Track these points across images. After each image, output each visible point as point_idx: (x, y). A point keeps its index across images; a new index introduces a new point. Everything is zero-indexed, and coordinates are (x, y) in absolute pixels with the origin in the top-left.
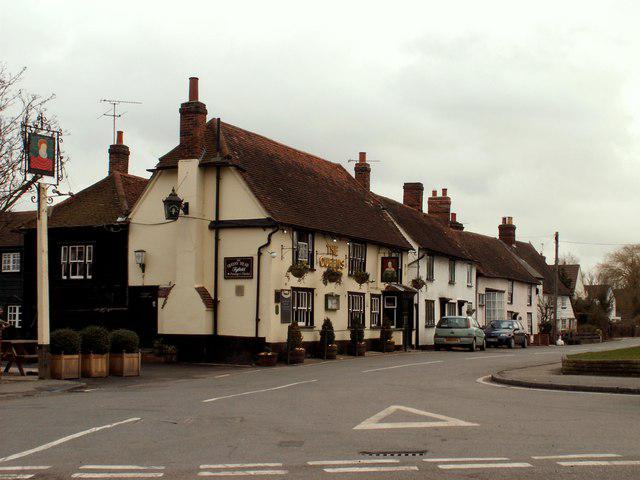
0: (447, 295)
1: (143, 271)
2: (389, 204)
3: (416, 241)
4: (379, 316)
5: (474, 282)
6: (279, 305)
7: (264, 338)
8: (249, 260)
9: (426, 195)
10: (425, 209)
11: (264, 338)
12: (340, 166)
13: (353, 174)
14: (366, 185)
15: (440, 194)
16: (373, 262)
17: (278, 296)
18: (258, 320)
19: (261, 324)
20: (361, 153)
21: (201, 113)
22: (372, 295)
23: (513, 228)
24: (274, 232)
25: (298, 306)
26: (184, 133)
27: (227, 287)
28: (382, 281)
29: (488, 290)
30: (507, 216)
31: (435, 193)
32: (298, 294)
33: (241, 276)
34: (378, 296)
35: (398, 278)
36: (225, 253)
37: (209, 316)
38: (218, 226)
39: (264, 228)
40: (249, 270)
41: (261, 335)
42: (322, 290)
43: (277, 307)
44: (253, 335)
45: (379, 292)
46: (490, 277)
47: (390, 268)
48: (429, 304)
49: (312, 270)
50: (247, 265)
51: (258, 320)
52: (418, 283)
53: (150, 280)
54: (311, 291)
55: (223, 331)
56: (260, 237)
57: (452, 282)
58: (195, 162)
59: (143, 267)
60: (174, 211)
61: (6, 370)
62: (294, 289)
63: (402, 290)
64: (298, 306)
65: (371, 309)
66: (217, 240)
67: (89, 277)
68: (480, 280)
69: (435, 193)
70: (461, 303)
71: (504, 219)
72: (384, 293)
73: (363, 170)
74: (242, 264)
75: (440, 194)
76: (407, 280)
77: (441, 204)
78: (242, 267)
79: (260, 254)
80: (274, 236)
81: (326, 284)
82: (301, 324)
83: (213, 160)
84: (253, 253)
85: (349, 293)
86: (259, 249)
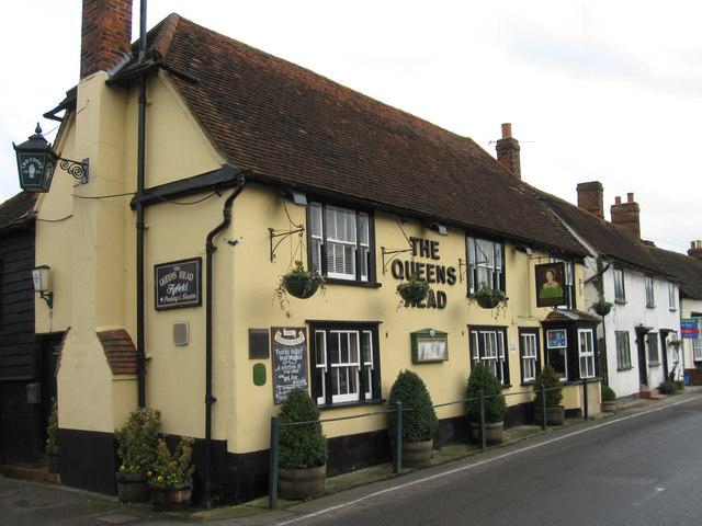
0: (647, 325)
1: (51, 307)
4: (538, 363)
6: (268, 363)
8: (191, 264)
9: (608, 202)
10: (608, 217)
13: (494, 154)
15: (624, 200)
16: (520, 271)
17: (260, 343)
18: (210, 401)
19: (218, 410)
20: (503, 125)
22: (522, 330)
27: (161, 326)
28: (539, 306)
30: (695, 240)
31: (618, 199)
32: (481, 336)
33: (182, 306)
34: (534, 330)
35: (567, 296)
36: (160, 253)
37: (129, 387)
38: (147, 200)
40: (194, 287)
41: (218, 435)
42: (400, 322)
44: (203, 436)
45: (537, 325)
47: (551, 284)
48: (622, 338)
50: (190, 277)
51: (210, 401)
52: (603, 309)
56: (209, 212)
57: (650, 306)
61: (329, 400)
64: (332, 358)
65: (522, 353)
66: (142, 229)
68: (685, 302)
69: (618, 199)
70: (664, 333)
71: (693, 243)
72: (546, 325)
73: (508, 147)
74: (183, 275)
76: (584, 301)
77: (628, 212)
79: (211, 249)
80: (236, 202)
81: (380, 285)
84: (199, 250)
85: (471, 327)
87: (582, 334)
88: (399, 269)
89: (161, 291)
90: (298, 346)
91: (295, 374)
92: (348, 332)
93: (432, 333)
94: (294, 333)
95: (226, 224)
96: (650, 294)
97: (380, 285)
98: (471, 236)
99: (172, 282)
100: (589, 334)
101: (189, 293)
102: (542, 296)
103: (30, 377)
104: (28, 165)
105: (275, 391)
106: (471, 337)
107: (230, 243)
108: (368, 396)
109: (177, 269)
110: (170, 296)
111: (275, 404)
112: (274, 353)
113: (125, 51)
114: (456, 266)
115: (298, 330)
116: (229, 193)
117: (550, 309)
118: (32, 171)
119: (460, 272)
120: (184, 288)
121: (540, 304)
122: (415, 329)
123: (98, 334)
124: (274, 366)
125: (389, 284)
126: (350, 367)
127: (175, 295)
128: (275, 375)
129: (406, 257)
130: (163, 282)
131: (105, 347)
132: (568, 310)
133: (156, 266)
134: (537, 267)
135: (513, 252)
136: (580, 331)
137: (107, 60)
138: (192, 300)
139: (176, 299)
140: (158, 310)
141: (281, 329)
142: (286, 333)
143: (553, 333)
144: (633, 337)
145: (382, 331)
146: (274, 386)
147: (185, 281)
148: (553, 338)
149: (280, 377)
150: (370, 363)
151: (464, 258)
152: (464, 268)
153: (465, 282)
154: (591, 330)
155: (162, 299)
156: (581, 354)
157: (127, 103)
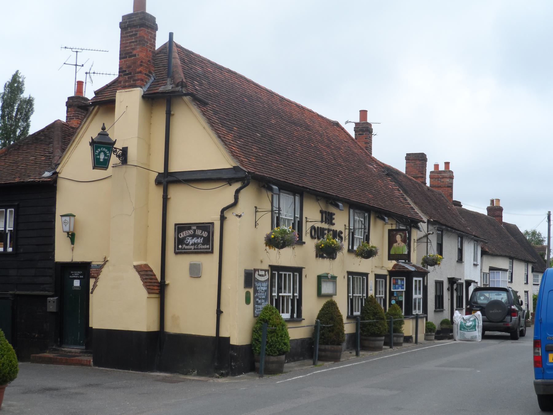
1: (73, 242)
2: (390, 172)
3: (425, 212)
5: (479, 262)
6: (251, 291)
7: (228, 339)
8: (207, 227)
9: (430, 168)
11: (228, 339)
12: (337, 124)
13: (353, 134)
14: (368, 147)
18: (219, 312)
19: (224, 319)
21: (147, 27)
22: (377, 276)
23: (501, 209)
24: (241, 188)
25: (279, 290)
26: (124, 54)
29: (491, 269)
31: (437, 166)
32: (280, 276)
34: (383, 277)
37: (155, 304)
39: (230, 181)
40: (208, 240)
41: (224, 334)
43: (248, 294)
44: (214, 334)
45: (385, 272)
46: (494, 255)
48: (439, 284)
49: (301, 242)
50: (205, 234)
51: (219, 312)
53: (79, 257)
54: (299, 270)
55: (170, 328)
58: (137, 93)
59: (72, 236)
60: (102, 157)
62: (273, 268)
63: (413, 269)
66: (165, 199)
67: (10, 250)
68: (485, 258)
69: (437, 166)
70: (469, 283)
71: (492, 201)
72: (392, 273)
74: (199, 232)
75: (442, 168)
76: (416, 259)
78: (198, 237)
79: (223, 218)
80: (242, 191)
81: (304, 243)
82: (286, 316)
83: (161, 89)
84: (215, 218)
85: (349, 273)
86: (223, 211)
87: (416, 281)
88: (317, 233)
89: (179, 241)
90: (265, 281)
91: (264, 299)
92: (287, 273)
93: (329, 276)
94: (263, 273)
95: (235, 204)
96: (460, 251)
97: (304, 243)
98: (352, 208)
99: (190, 236)
100: (420, 281)
101: (203, 244)
102: (392, 252)
103: (51, 293)
104: (101, 151)
105: (254, 308)
106: (349, 279)
107: (237, 215)
108: (295, 315)
109: (194, 228)
110: (187, 245)
111: (255, 317)
112: (255, 285)
113: (151, 73)
114: (343, 231)
115: (265, 271)
116: (237, 186)
117: (394, 262)
118: (102, 157)
119: (345, 234)
120: (200, 240)
121: (391, 257)
122: (319, 274)
123: (135, 267)
124: (254, 293)
125: (310, 244)
126: (287, 296)
127: (192, 245)
128: (255, 298)
129: (318, 225)
130: (182, 235)
131: (141, 276)
132: (405, 263)
133: (176, 225)
134: (389, 230)
135: (375, 219)
136: (415, 279)
137: (142, 80)
138: (206, 249)
139: (193, 247)
140: (176, 253)
141: (258, 270)
142: (261, 273)
143: (396, 279)
144: (446, 285)
145: (304, 272)
146: (254, 306)
147: (201, 237)
148: (396, 284)
149: (257, 300)
150: (296, 294)
151: (347, 225)
152: (347, 231)
153: (347, 241)
154: (421, 279)
155: (180, 246)
156: (414, 296)
157: (152, 106)
